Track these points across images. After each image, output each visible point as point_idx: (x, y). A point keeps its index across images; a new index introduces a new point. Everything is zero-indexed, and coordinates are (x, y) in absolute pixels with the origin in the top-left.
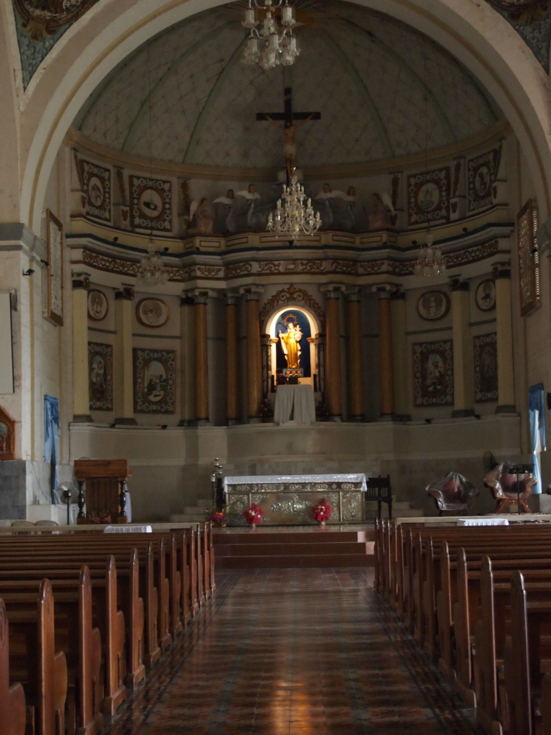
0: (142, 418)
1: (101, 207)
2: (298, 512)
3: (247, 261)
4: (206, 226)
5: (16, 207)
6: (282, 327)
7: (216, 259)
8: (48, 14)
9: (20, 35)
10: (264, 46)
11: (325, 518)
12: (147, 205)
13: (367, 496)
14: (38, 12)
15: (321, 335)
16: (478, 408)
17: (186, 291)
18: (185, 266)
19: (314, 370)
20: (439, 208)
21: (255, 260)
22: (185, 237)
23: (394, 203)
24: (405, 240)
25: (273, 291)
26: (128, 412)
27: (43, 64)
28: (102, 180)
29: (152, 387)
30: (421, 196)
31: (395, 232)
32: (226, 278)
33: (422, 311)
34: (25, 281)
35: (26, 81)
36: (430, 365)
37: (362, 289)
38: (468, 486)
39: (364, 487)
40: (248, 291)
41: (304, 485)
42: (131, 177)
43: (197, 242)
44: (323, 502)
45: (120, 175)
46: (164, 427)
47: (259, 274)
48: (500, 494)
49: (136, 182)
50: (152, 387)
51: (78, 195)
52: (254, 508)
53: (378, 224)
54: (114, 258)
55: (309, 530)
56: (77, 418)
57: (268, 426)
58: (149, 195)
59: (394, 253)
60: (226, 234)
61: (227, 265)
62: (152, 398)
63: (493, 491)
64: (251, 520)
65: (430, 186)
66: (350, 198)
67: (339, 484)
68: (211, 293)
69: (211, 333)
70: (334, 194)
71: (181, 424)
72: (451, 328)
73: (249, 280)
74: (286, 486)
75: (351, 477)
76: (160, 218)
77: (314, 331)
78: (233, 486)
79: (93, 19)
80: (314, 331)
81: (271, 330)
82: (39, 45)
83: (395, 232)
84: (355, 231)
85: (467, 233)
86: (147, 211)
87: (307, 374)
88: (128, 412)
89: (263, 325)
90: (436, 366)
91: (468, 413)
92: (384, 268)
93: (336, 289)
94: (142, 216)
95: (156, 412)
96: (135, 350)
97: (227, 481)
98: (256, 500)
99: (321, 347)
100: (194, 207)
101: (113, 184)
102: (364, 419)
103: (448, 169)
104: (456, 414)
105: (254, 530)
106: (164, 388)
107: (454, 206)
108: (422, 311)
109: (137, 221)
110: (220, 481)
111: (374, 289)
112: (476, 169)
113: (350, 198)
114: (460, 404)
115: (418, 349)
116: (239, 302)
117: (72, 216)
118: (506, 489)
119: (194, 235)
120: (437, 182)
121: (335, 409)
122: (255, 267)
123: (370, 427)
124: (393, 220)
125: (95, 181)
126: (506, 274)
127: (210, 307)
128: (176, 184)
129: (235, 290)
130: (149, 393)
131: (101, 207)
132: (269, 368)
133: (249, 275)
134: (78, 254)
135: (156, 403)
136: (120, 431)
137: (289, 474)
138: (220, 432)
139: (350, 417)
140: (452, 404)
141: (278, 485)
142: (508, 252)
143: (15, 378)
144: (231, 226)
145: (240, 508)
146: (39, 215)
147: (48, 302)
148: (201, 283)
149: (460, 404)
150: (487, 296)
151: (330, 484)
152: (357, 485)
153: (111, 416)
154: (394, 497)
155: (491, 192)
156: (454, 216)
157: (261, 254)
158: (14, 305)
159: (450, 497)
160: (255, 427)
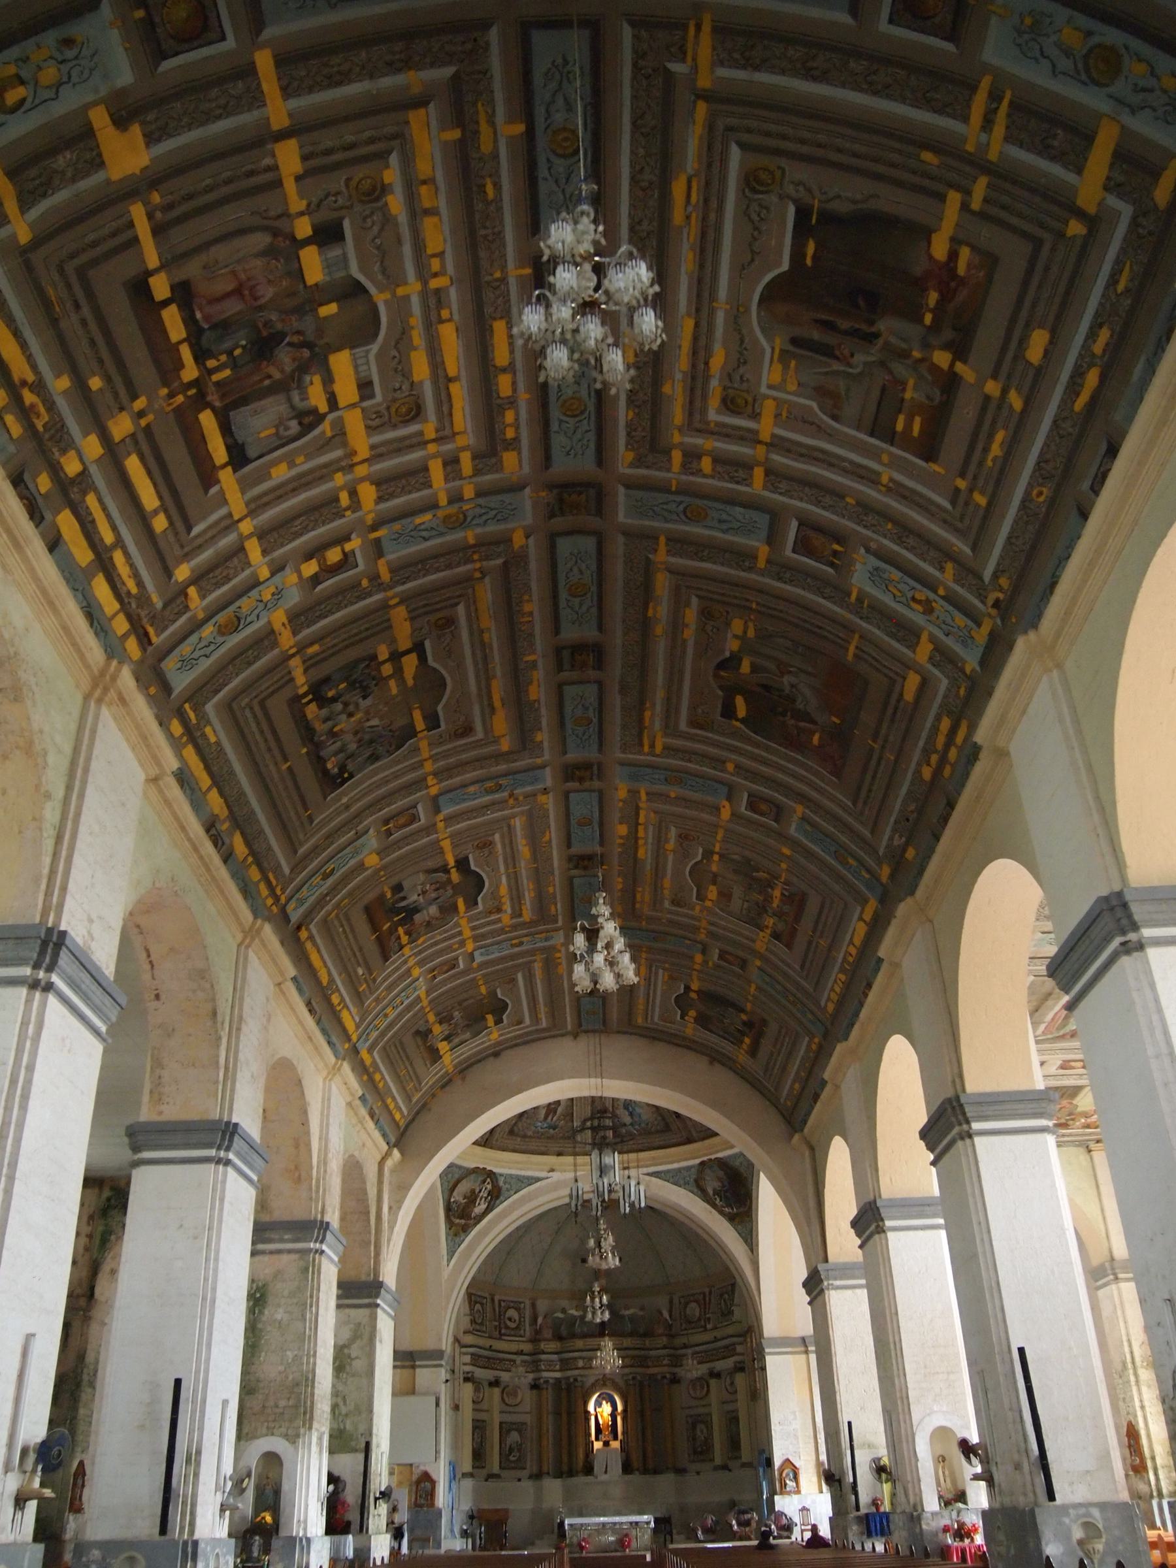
0: (504, 1474)
1: (482, 1324)
2: (612, 1542)
3: (575, 1359)
4: (547, 1334)
5: (440, 1339)
6: (598, 1404)
7: (555, 1357)
8: (463, 1222)
9: (447, 1234)
10: (594, 1313)
11: (629, 1546)
12: (510, 1319)
13: (655, 1530)
14: (457, 1221)
15: (625, 1411)
16: (731, 1464)
17: (535, 1379)
18: (534, 1362)
19: (620, 1436)
20: (699, 1319)
21: (580, 1358)
22: (534, 1340)
23: (670, 1316)
24: (679, 1341)
25: (591, 1380)
26: (496, 1469)
27: (460, 1250)
28: (482, 1304)
29: (511, 1450)
30: (688, 1311)
31: (671, 1336)
32: (561, 1370)
33: (692, 1392)
34: (443, 1386)
35: (449, 1261)
36: (699, 1433)
37: (652, 1376)
38: (716, 1523)
39: (652, 1525)
40: (576, 1380)
41: (615, 1524)
42: (500, 1301)
43: (542, 1345)
44: (627, 1535)
45: (493, 1300)
46: (519, 1480)
47: (583, 1368)
48: (736, 1527)
49: (503, 1304)
50: (511, 1450)
51: (468, 1319)
52: (584, 1540)
53: (660, 1331)
54: (489, 1358)
55: (619, 1554)
56: (464, 1475)
57: (590, 1479)
58: (512, 1313)
59: (672, 1351)
60: (560, 1338)
61: (561, 1360)
62: (512, 1458)
63: (731, 1526)
64: (582, 1548)
65: (693, 1305)
66: (641, 1313)
67: (637, 1523)
68: (551, 1381)
69: (550, 1409)
70: (631, 1311)
71: (530, 1477)
72: (710, 1405)
73: (576, 1372)
74: (604, 1524)
75: (645, 1518)
76: (517, 1328)
77: (620, 1408)
78: (571, 1525)
79: (488, 1222)
80: (620, 1408)
81: (591, 1407)
82: (457, 1240)
83: (671, 1336)
84: (645, 1335)
85: (716, 1340)
86: (509, 1323)
87: (616, 1438)
88: (496, 1469)
89: (586, 1403)
90: (702, 1431)
91: (725, 1467)
92: (665, 1362)
93: (634, 1378)
94: (507, 1327)
95: (513, 1468)
96: (501, 1423)
97: (567, 1522)
98: (585, 1534)
99: (624, 1419)
100: (540, 1320)
101: (489, 1308)
102: (656, 1472)
103: (704, 1294)
104: (716, 1468)
105: (584, 1554)
106: (519, 1450)
107: (709, 1319)
108: (692, 1392)
109: (503, 1331)
110: (562, 1524)
111: (659, 1377)
112: (721, 1295)
113: (641, 1313)
114: (718, 1461)
115: (690, 1421)
116: (569, 1389)
117: (465, 1333)
118: (739, 1524)
119: (540, 1341)
120: (696, 1301)
121: (635, 1465)
122: (581, 1363)
123: (661, 1478)
124: (670, 1326)
125: (478, 1306)
126: (742, 1369)
127: (550, 1390)
128: (528, 1303)
129: (568, 1378)
130: (510, 1454)
131: (482, 1324)
132: (590, 1435)
133: (577, 1368)
134: (467, 1359)
135: (514, 1462)
136: (491, 1484)
137: (604, 1516)
138: (558, 1482)
139: (645, 1471)
140: (712, 1460)
141: (598, 1524)
142: (742, 1354)
143: (437, 1452)
144: (564, 1331)
145: (575, 1540)
146: (451, 1339)
147: (453, 1398)
148: (545, 1374)
149: (718, 1461)
150: (732, 1383)
151: (631, 1523)
152: (648, 1523)
153: (484, 1472)
154: (674, 1531)
155: (731, 1313)
156: (709, 1327)
157: (584, 1354)
158: (437, 1405)
159: (706, 1531)
160: (581, 1480)
